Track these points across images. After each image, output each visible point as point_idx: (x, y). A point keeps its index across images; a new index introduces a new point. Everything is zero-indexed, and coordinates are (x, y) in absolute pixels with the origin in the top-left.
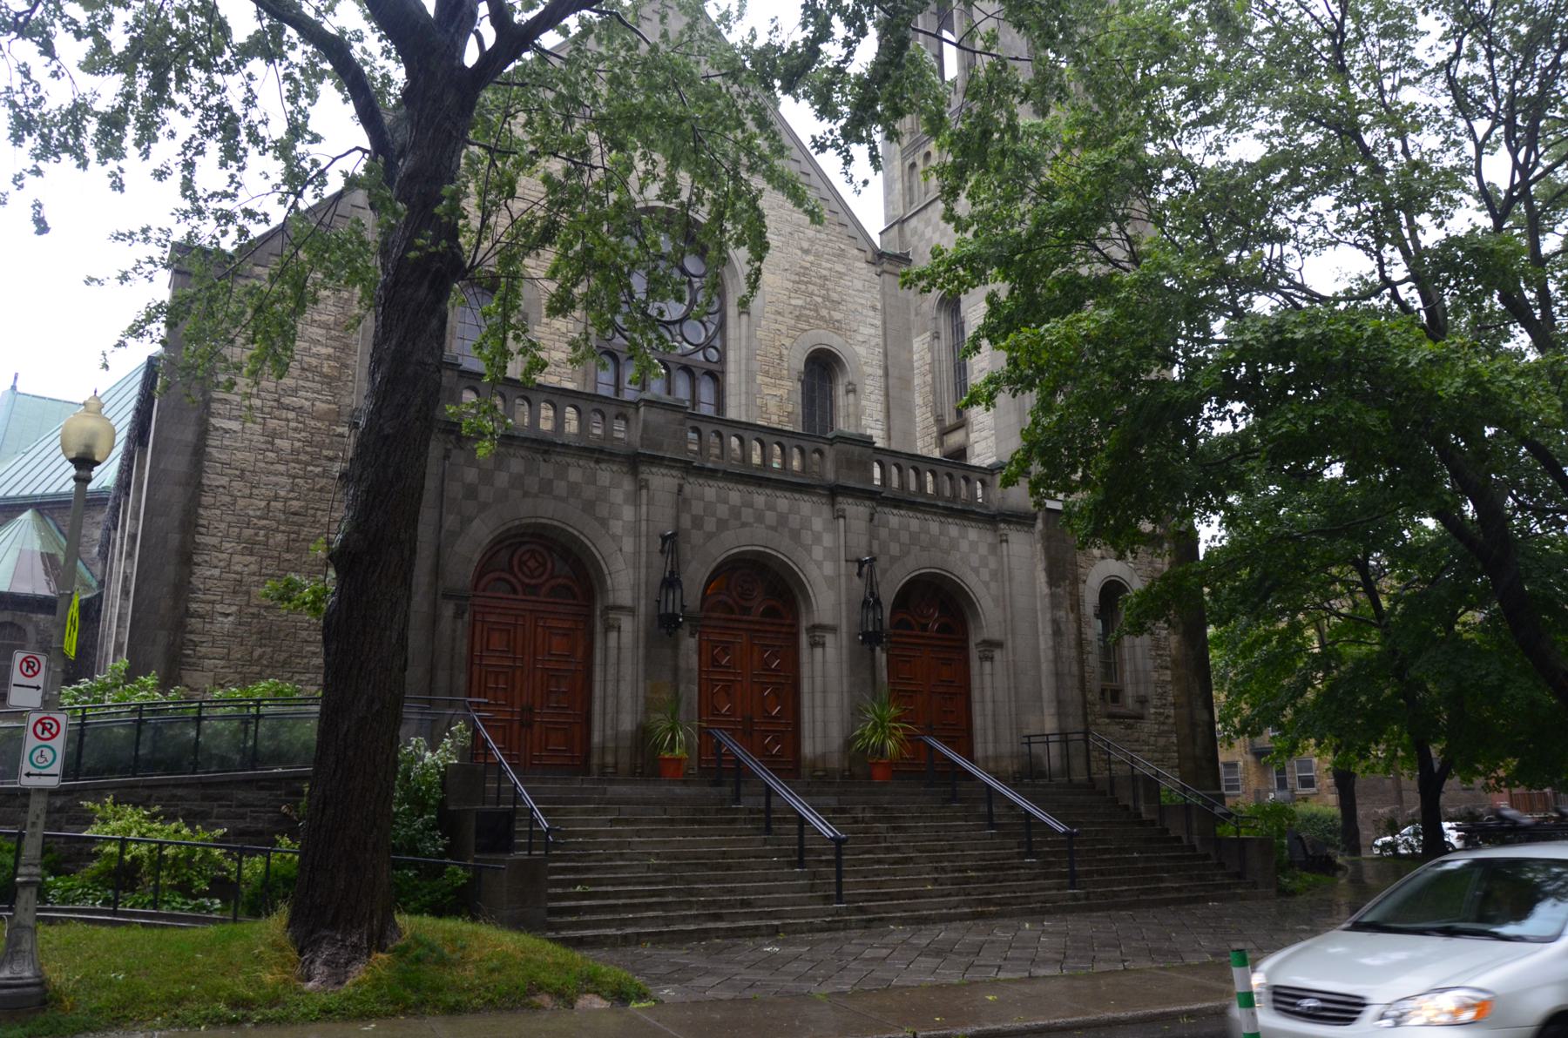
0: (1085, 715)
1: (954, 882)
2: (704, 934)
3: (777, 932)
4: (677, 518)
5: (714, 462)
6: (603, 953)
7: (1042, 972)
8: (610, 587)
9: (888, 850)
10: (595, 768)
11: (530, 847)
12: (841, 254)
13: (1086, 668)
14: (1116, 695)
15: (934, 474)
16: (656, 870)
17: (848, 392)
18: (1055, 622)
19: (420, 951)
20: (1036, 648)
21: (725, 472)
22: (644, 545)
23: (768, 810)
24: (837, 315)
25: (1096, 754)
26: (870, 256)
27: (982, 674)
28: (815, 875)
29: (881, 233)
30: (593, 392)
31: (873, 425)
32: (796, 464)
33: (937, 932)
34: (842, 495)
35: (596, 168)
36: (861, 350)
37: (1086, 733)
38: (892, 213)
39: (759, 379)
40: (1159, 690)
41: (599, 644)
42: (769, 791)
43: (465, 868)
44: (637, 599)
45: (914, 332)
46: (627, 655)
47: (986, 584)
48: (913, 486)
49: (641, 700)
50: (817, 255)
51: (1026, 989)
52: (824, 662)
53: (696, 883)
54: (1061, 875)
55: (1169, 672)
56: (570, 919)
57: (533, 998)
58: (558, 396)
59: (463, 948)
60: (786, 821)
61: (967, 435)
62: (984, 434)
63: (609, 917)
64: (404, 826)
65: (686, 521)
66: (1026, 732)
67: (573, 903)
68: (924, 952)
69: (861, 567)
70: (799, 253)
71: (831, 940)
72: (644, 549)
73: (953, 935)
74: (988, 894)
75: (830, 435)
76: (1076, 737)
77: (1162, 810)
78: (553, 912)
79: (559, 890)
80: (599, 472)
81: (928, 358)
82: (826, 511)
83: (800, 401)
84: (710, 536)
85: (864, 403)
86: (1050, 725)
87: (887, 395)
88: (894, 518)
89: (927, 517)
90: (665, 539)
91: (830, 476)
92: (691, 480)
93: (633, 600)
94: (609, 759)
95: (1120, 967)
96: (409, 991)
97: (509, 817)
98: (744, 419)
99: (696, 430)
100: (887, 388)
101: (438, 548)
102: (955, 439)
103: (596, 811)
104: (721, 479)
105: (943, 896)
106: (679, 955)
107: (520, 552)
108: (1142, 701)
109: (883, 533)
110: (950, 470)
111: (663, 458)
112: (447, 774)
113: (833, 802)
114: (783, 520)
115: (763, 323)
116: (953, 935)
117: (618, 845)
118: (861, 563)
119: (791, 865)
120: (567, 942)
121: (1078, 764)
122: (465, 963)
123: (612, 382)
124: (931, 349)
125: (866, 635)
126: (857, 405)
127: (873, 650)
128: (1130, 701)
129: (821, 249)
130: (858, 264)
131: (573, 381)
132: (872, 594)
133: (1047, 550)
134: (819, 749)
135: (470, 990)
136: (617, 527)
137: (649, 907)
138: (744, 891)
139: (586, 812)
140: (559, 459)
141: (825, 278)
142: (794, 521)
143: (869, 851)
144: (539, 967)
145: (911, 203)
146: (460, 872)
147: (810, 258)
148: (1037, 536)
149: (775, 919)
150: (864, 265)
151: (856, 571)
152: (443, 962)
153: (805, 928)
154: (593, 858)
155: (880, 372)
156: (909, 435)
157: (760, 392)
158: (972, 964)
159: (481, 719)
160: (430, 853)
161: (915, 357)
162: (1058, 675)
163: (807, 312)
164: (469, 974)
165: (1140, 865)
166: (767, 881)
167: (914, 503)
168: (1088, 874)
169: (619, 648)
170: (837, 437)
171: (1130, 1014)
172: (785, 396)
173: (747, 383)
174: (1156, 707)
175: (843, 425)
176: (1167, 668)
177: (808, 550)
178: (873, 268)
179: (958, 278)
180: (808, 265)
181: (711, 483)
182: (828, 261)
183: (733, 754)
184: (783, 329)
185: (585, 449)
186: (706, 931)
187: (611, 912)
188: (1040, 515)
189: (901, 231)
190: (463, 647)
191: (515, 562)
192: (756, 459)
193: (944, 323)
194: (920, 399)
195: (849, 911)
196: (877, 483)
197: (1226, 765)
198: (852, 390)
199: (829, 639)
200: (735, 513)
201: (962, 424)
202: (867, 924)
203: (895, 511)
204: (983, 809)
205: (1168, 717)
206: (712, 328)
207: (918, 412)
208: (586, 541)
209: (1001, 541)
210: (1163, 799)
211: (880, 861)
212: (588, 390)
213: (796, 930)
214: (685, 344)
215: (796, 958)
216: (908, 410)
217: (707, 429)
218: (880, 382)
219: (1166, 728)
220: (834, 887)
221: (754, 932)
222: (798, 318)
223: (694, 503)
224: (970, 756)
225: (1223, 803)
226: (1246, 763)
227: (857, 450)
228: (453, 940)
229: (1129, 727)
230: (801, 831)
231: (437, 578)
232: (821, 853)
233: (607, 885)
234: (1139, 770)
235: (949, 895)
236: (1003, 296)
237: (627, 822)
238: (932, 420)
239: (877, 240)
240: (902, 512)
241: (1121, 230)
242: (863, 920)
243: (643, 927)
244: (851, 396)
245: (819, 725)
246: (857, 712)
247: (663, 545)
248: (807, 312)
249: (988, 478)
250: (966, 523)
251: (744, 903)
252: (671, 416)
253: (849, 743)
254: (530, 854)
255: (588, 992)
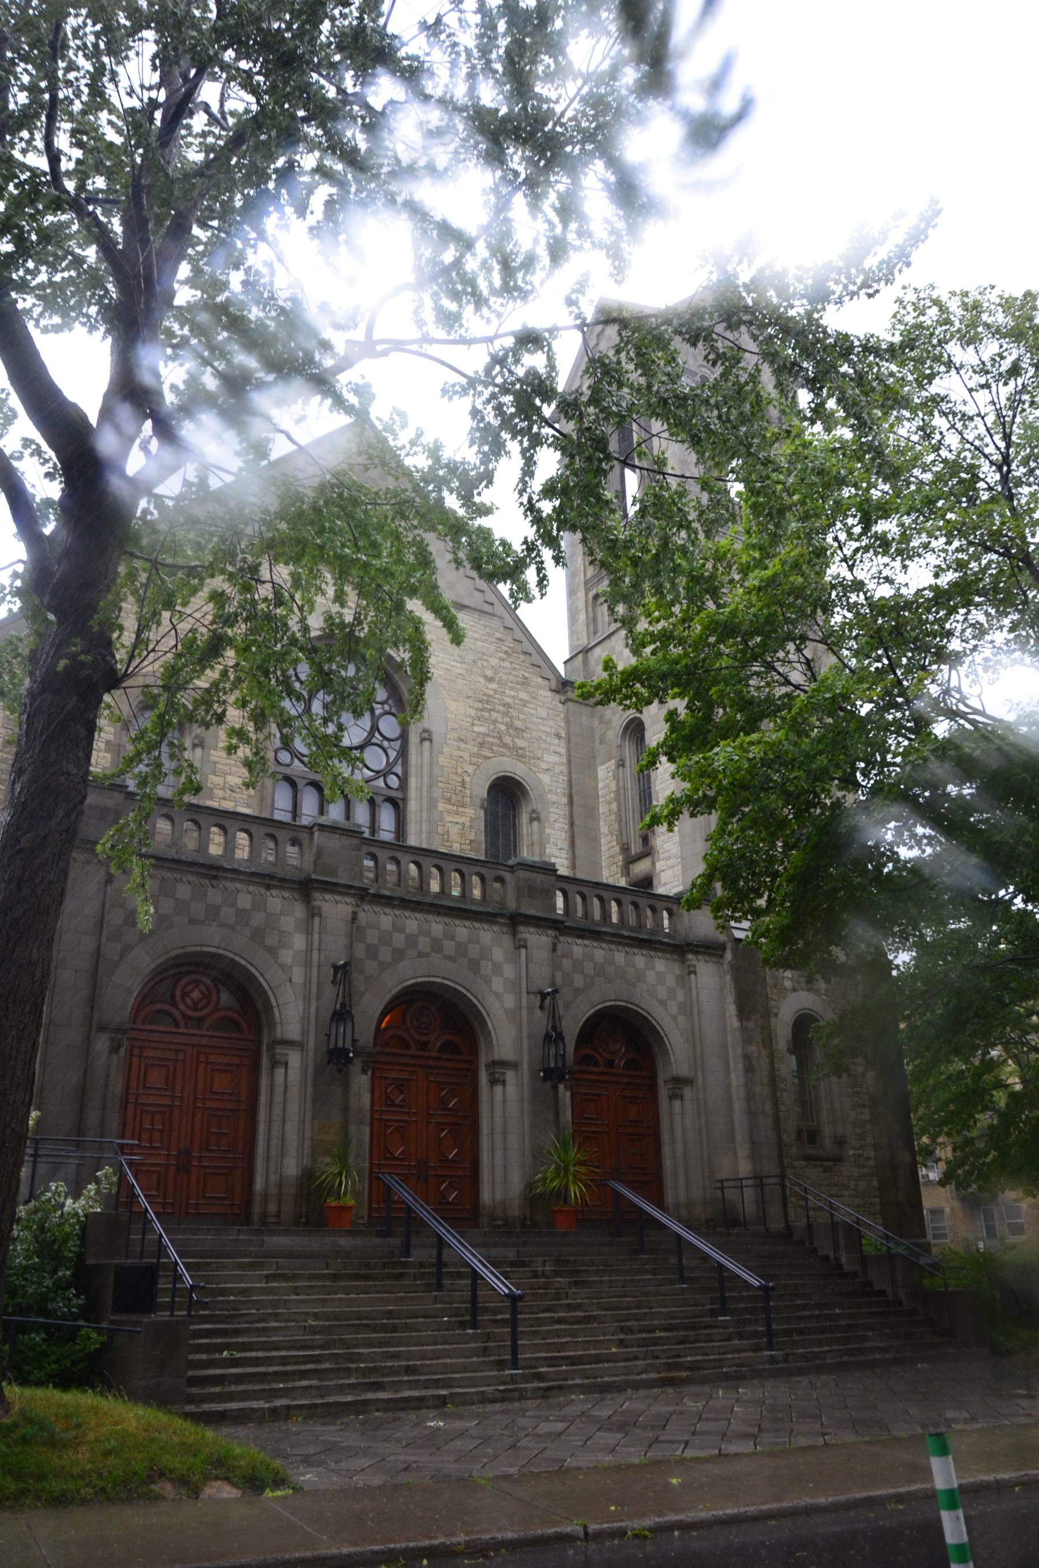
0: (781, 1157)
1: (642, 1343)
2: (362, 1407)
3: (445, 1403)
4: (350, 947)
5: (390, 889)
6: (241, 1431)
7: (733, 1449)
8: (278, 1020)
9: (569, 1307)
10: (256, 1218)
11: (172, 1307)
12: (525, 683)
13: (782, 1108)
14: (812, 1136)
15: (619, 903)
16: (314, 1333)
17: (532, 820)
18: (746, 1057)
19: (28, 1430)
20: (729, 1086)
21: (402, 900)
22: (315, 974)
23: (440, 1264)
24: (520, 743)
25: (793, 1199)
26: (554, 684)
27: (671, 1114)
28: (488, 1337)
29: (565, 663)
30: (268, 816)
31: (557, 853)
32: (477, 893)
33: (621, 1401)
34: (523, 923)
35: (264, 582)
36: (546, 778)
37: (783, 1177)
38: (575, 642)
39: (441, 806)
40: (858, 1130)
41: (264, 1082)
42: (441, 1243)
43: (99, 1331)
44: (305, 1032)
45: (598, 761)
46: (294, 1093)
47: (674, 1018)
48: (597, 915)
49: (307, 1144)
50: (500, 683)
51: (715, 1469)
52: (504, 1102)
53: (356, 1347)
54: (756, 1335)
55: (867, 1111)
56: (213, 1390)
57: (153, 1487)
58: (226, 819)
59: (79, 1426)
60: (459, 1275)
61: (654, 864)
62: (671, 862)
63: (257, 1387)
64: (33, 1283)
65: (360, 951)
66: (720, 1176)
67: (218, 1372)
68: (605, 1426)
69: (543, 999)
70: (483, 680)
71: (504, 1412)
72: (315, 980)
73: (639, 1406)
74: (679, 1356)
75: (511, 862)
76: (772, 1180)
77: (864, 1260)
78: (192, 1381)
79: (204, 1357)
80: (270, 899)
81: (613, 786)
82: (507, 941)
83: (483, 828)
84: (383, 966)
85: (547, 831)
86: (744, 1168)
87: (572, 824)
88: (578, 948)
89: (613, 947)
90: (336, 968)
91: (512, 905)
92: (367, 907)
93: (303, 1033)
94: (272, 1208)
95: (820, 1441)
96: (9, 1478)
97: (150, 1274)
98: (424, 846)
99: (374, 857)
100: (571, 816)
101: (95, 975)
102: (641, 868)
103: (252, 1266)
104: (399, 907)
105: (629, 1360)
106: (330, 1432)
107: (183, 982)
108: (840, 1142)
109: (567, 963)
110: (635, 899)
111: (336, 884)
112: (88, 1224)
113: (511, 1254)
114: (462, 949)
115: (445, 750)
116: (639, 1406)
117: (274, 1304)
118: (543, 996)
119: (462, 1325)
120: (197, 1418)
121: (774, 1210)
122: (78, 1444)
123: (290, 809)
124: (616, 777)
125: (548, 1071)
126: (541, 833)
127: (555, 1088)
128: (827, 1142)
129: (505, 677)
130: (542, 692)
131: (248, 806)
132: (554, 1028)
133: (737, 982)
134: (499, 1196)
135: (81, 1477)
136: (286, 956)
137: (303, 1375)
138: (410, 1356)
139: (241, 1266)
140: (228, 884)
141: (508, 705)
142: (473, 951)
143: (549, 1310)
144: (162, 1448)
145: (595, 633)
146: (94, 1335)
147: (494, 686)
148: (726, 967)
149: (443, 1388)
150: (549, 693)
151: (538, 1003)
152: (53, 1443)
153: (475, 1398)
154: (245, 1319)
155: (565, 800)
156: (597, 866)
157: (442, 819)
158: (656, 1440)
159: (130, 1164)
160: (63, 1314)
161: (600, 785)
162: (751, 1114)
163: (490, 739)
164: (82, 1458)
165: (843, 1323)
166: (435, 1344)
167: (600, 933)
168: (787, 1332)
169: (286, 1086)
170: (519, 864)
171: (830, 1499)
172: (468, 824)
173: (430, 809)
174: (855, 1148)
175: (526, 853)
176: (864, 1106)
177: (488, 981)
178: (557, 697)
179: (636, 694)
180: (492, 693)
181: (387, 910)
182: (512, 689)
183: (404, 1202)
184: (466, 756)
185: (253, 874)
186: (365, 1403)
187: (263, 1382)
188: (729, 946)
189: (585, 661)
190: (117, 1086)
191: (178, 994)
192: (435, 886)
193: (628, 750)
194: (605, 827)
195: (525, 1378)
196: (560, 912)
197: (933, 1212)
198: (535, 817)
199: (510, 1075)
200: (412, 941)
201: (648, 851)
202: (545, 1393)
203: (579, 941)
204: (673, 1261)
205: (868, 1159)
206: (393, 754)
207: (603, 841)
208: (254, 971)
209: (690, 973)
210: (865, 1248)
211: (560, 1321)
212: (263, 815)
213: (466, 1401)
214: (365, 770)
215: (462, 1434)
216: (594, 841)
217: (383, 855)
218: (564, 810)
219: (866, 1171)
220: (509, 1350)
221: (420, 1403)
222: (481, 745)
223: (369, 931)
224: (660, 1205)
225: (929, 1252)
226: (952, 1209)
227: (539, 878)
228: (68, 1417)
229: (826, 1170)
230: (474, 1287)
231: (92, 1009)
232: (495, 1312)
233: (258, 1350)
234: (839, 1217)
235: (636, 1358)
236: (683, 713)
237: (285, 1278)
238: (617, 848)
239: (561, 669)
240: (586, 942)
241: (799, 650)
242: (540, 1389)
243: (295, 1399)
244: (535, 824)
245: (499, 1170)
246: (538, 1155)
247: (335, 975)
248: (490, 739)
249: (675, 907)
250: (652, 953)
251: (409, 1370)
252: (346, 841)
253: (530, 1186)
254: (172, 1315)
255: (217, 1478)
